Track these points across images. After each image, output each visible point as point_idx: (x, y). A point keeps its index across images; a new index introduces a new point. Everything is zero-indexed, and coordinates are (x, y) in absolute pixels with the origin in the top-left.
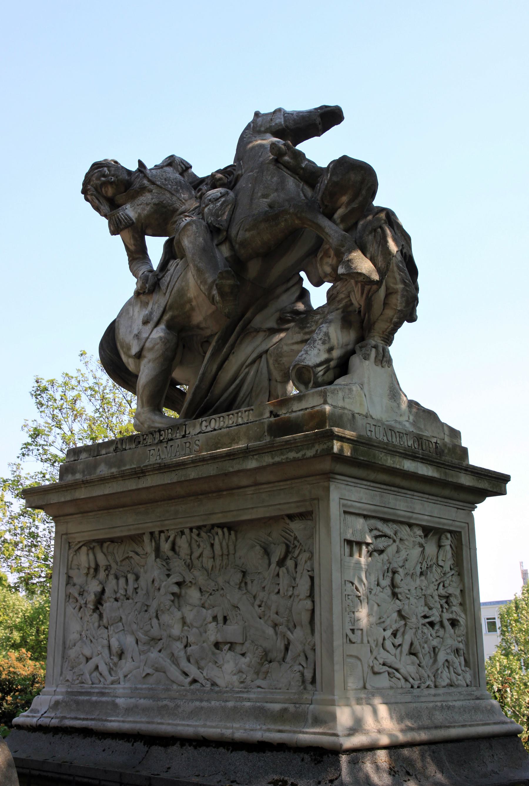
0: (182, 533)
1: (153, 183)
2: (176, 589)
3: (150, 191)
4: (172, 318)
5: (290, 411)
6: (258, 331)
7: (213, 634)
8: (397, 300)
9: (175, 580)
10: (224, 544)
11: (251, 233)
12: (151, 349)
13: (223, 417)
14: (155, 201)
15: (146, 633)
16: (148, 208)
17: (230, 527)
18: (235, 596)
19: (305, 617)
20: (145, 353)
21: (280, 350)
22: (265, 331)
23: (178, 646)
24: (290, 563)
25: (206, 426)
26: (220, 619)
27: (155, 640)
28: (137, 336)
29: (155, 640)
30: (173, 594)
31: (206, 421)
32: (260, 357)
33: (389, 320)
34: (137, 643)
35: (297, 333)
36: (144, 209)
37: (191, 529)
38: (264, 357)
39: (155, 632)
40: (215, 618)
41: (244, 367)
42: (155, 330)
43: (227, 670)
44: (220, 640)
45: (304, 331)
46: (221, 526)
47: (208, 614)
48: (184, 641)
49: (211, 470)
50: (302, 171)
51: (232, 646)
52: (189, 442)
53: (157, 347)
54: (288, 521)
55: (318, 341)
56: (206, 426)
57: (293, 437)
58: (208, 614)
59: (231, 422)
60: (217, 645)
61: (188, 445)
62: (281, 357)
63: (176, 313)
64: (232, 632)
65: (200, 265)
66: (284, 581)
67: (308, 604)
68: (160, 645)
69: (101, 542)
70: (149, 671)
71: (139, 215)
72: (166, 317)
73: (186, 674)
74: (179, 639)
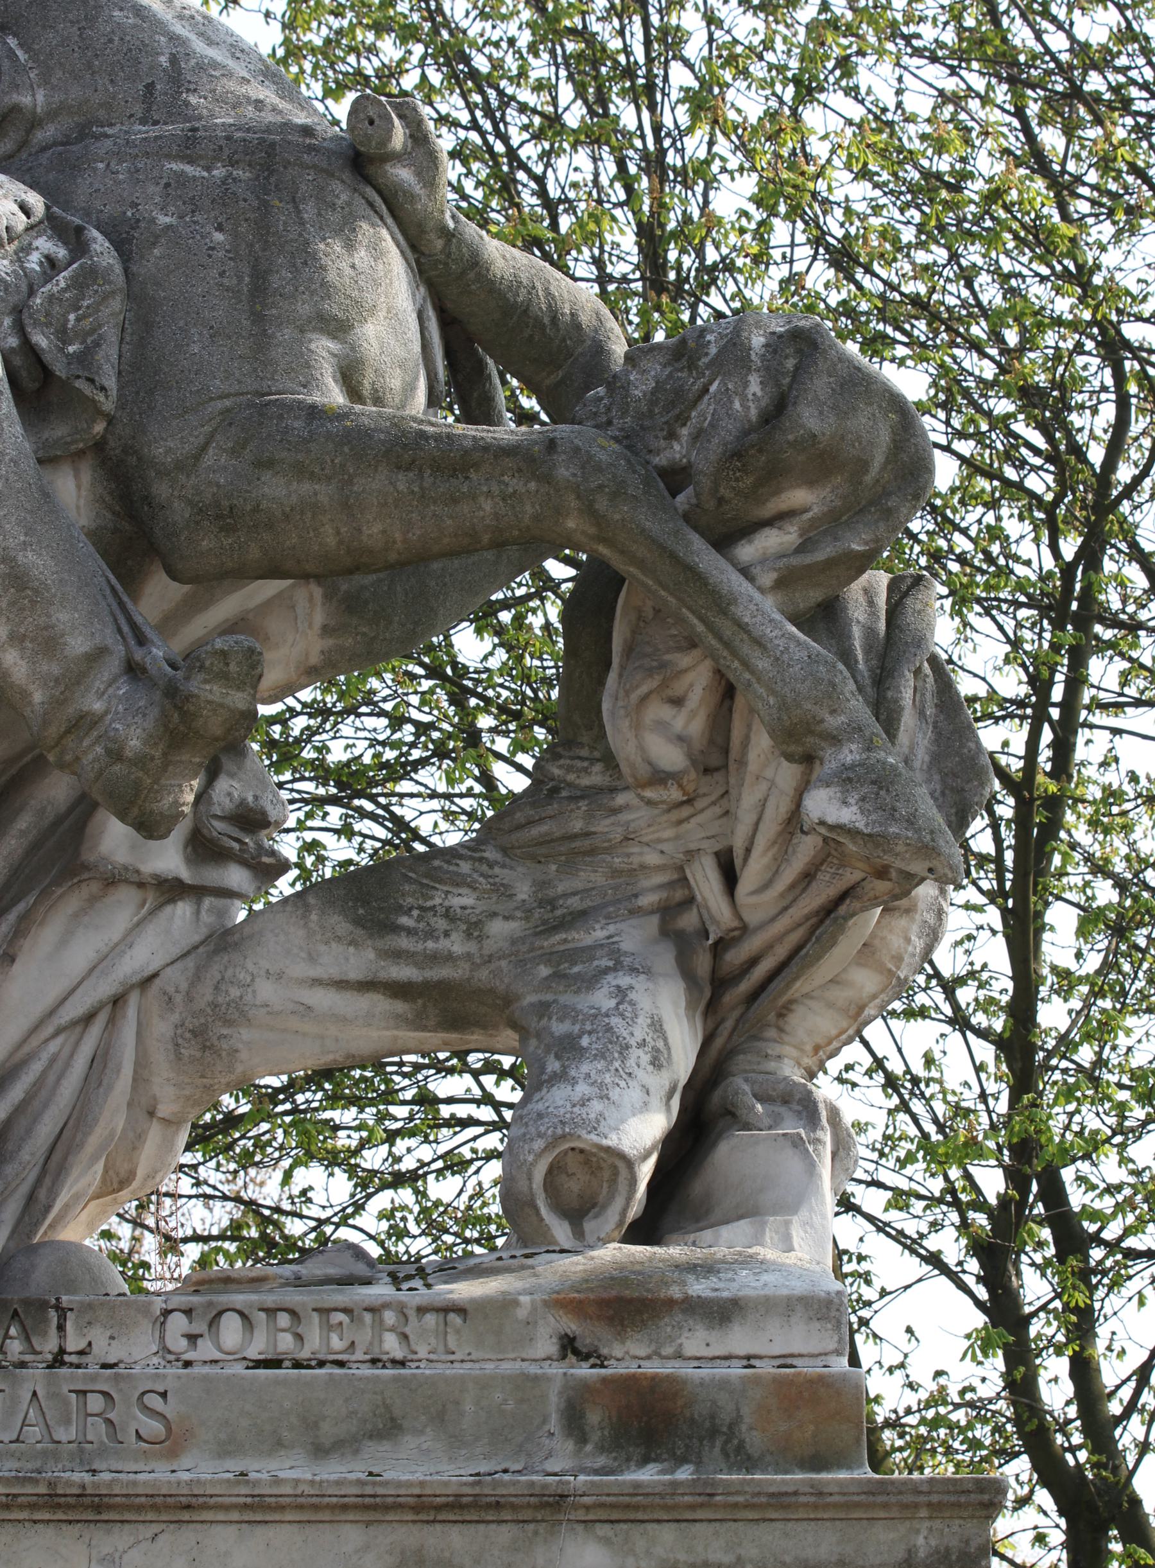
5: (668, 1350)
6: (113, 880)
8: (908, 940)
13: (293, 1313)
21: (235, 992)
22: (141, 885)
25: (192, 1338)
31: (188, 1312)
32: (117, 1001)
33: (852, 1012)
35: (339, 939)
38: (133, 999)
41: (49, 1030)
45: (380, 944)
50: (439, 244)
52: (105, 1394)
55: (635, 1053)
56: (192, 1338)
57: (812, 1484)
59: (336, 1343)
61: (95, 1403)
62: (229, 1023)
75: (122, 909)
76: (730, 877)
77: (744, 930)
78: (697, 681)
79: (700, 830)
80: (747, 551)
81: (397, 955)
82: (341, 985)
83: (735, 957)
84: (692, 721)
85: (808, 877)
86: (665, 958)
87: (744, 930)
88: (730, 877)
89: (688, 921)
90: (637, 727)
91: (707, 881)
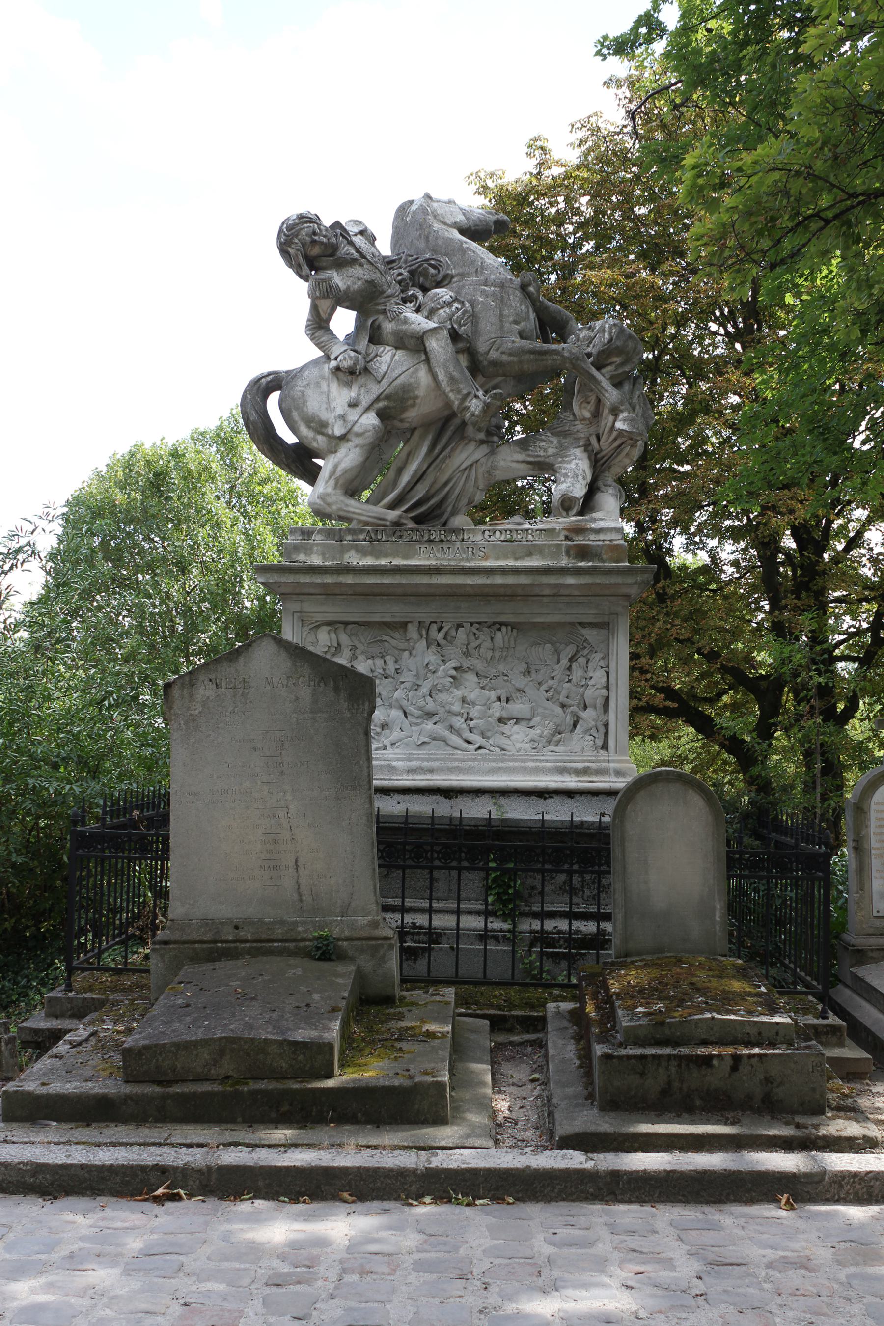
0: (459, 626)
1: (364, 257)
2: (454, 673)
3: (361, 265)
4: (385, 408)
7: (497, 710)
9: (454, 665)
10: (506, 638)
11: (512, 358)
12: (358, 435)
14: (367, 277)
15: (420, 709)
16: (360, 283)
17: (513, 626)
18: (520, 682)
19: (600, 702)
20: (349, 436)
23: (459, 722)
24: (582, 660)
26: (503, 698)
27: (430, 715)
28: (343, 417)
29: (430, 715)
30: (452, 677)
32: (471, 465)
34: (406, 716)
36: (354, 283)
37: (472, 624)
39: (431, 706)
40: (499, 699)
42: (365, 416)
44: (505, 715)
47: (493, 695)
48: (465, 715)
49: (524, 580)
51: (518, 720)
53: (368, 434)
54: (579, 628)
58: (493, 695)
60: (501, 720)
63: (392, 404)
64: (518, 707)
65: (455, 373)
66: (577, 673)
67: (604, 691)
68: (436, 718)
69: (346, 623)
70: (426, 740)
71: (348, 287)
72: (381, 404)
73: (469, 742)
74: (460, 714)
75: (472, 446)
76: (599, 440)
77: (601, 450)
78: (593, 399)
79: (592, 429)
80: (604, 371)
81: (529, 456)
82: (518, 462)
83: (599, 456)
84: (591, 407)
85: (615, 439)
86: (585, 456)
87: (601, 450)
88: (599, 440)
89: (590, 448)
90: (580, 408)
91: (594, 440)
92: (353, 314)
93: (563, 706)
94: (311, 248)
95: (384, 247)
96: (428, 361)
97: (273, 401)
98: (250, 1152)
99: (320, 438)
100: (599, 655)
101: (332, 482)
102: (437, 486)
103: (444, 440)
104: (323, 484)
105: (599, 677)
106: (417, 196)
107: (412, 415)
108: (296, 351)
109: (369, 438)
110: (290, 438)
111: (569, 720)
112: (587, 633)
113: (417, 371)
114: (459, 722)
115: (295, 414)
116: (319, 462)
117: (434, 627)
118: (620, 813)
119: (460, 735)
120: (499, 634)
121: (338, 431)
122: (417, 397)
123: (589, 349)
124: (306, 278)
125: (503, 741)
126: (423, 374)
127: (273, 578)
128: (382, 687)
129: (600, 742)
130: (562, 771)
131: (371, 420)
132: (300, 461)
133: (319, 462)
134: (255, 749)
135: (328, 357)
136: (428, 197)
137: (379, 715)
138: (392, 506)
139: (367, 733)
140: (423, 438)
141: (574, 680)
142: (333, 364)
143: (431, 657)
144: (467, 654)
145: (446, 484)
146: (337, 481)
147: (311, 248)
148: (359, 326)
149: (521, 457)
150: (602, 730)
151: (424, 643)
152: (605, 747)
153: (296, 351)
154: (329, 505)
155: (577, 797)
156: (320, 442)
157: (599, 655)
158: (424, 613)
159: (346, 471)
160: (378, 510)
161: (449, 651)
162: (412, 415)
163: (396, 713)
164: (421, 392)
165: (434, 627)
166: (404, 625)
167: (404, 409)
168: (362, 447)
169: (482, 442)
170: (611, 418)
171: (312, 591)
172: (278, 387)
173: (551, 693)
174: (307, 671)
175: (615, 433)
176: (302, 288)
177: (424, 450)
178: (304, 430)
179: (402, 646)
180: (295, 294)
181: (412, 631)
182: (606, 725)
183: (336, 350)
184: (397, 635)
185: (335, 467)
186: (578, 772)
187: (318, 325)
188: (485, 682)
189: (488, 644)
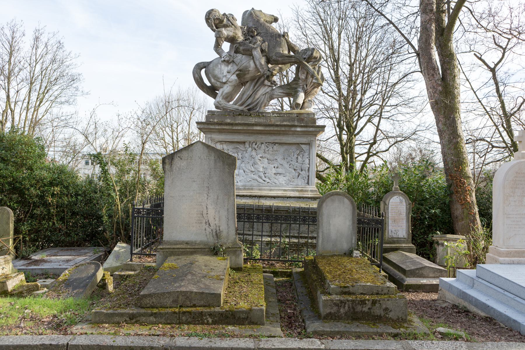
0: (262, 143)
2: (260, 159)
7: (274, 171)
12: (230, 82)
19: (307, 169)
23: (262, 175)
40: (274, 167)
43: (282, 180)
46: (277, 143)
58: (273, 166)
64: (280, 170)
68: (254, 173)
72: (237, 73)
75: (267, 87)
91: (305, 86)
92: (229, 44)
93: (295, 170)
94: (216, 22)
95: (239, 23)
96: (253, 58)
97: (203, 71)
98: (187, 339)
99: (218, 83)
100: (307, 154)
101: (221, 98)
102: (255, 99)
103: (257, 85)
104: (219, 98)
105: (307, 161)
106: (250, 9)
107: (248, 77)
108: (211, 56)
109: (234, 83)
110: (208, 84)
111: (297, 174)
112: (303, 146)
113: (249, 62)
114: (262, 175)
115: (210, 76)
116: (217, 92)
117: (254, 143)
118: (320, 206)
119: (261, 179)
120: (275, 146)
121: (224, 80)
122: (249, 71)
123: (305, 57)
124: (214, 31)
125: (276, 181)
126: (252, 63)
127: (202, 126)
128: (238, 163)
129: (306, 182)
130: (293, 191)
131: (234, 77)
132: (212, 91)
133: (217, 92)
134: (194, 181)
135: (221, 57)
136: (253, 9)
137: (236, 172)
138: (242, 105)
139: (233, 176)
140: (251, 84)
141: (299, 162)
142: (223, 59)
143: (254, 153)
144: (265, 152)
145: (258, 99)
146: (223, 97)
147: (216, 22)
148: (231, 47)
149: (281, 91)
150: (307, 178)
151: (250, 148)
152: (308, 183)
153: (211, 56)
154: (220, 105)
155: (305, 199)
156: (218, 84)
157: (307, 154)
158: (251, 138)
159: (226, 94)
160: (236, 107)
161: (259, 151)
162: (248, 77)
163: (242, 171)
164: (251, 69)
165: (254, 143)
166: (244, 143)
167: (245, 75)
168: (231, 86)
169: (270, 86)
170: (311, 79)
171: (214, 131)
172: (205, 67)
173: (291, 166)
174: (213, 154)
175: (312, 84)
176: (213, 34)
177: (252, 87)
178: (213, 80)
179: (243, 149)
180: (211, 36)
181: (247, 145)
182: (308, 176)
183: (224, 55)
184: (242, 146)
185: (223, 92)
186: (298, 191)
187: (217, 47)
188: (270, 162)
189: (271, 149)
